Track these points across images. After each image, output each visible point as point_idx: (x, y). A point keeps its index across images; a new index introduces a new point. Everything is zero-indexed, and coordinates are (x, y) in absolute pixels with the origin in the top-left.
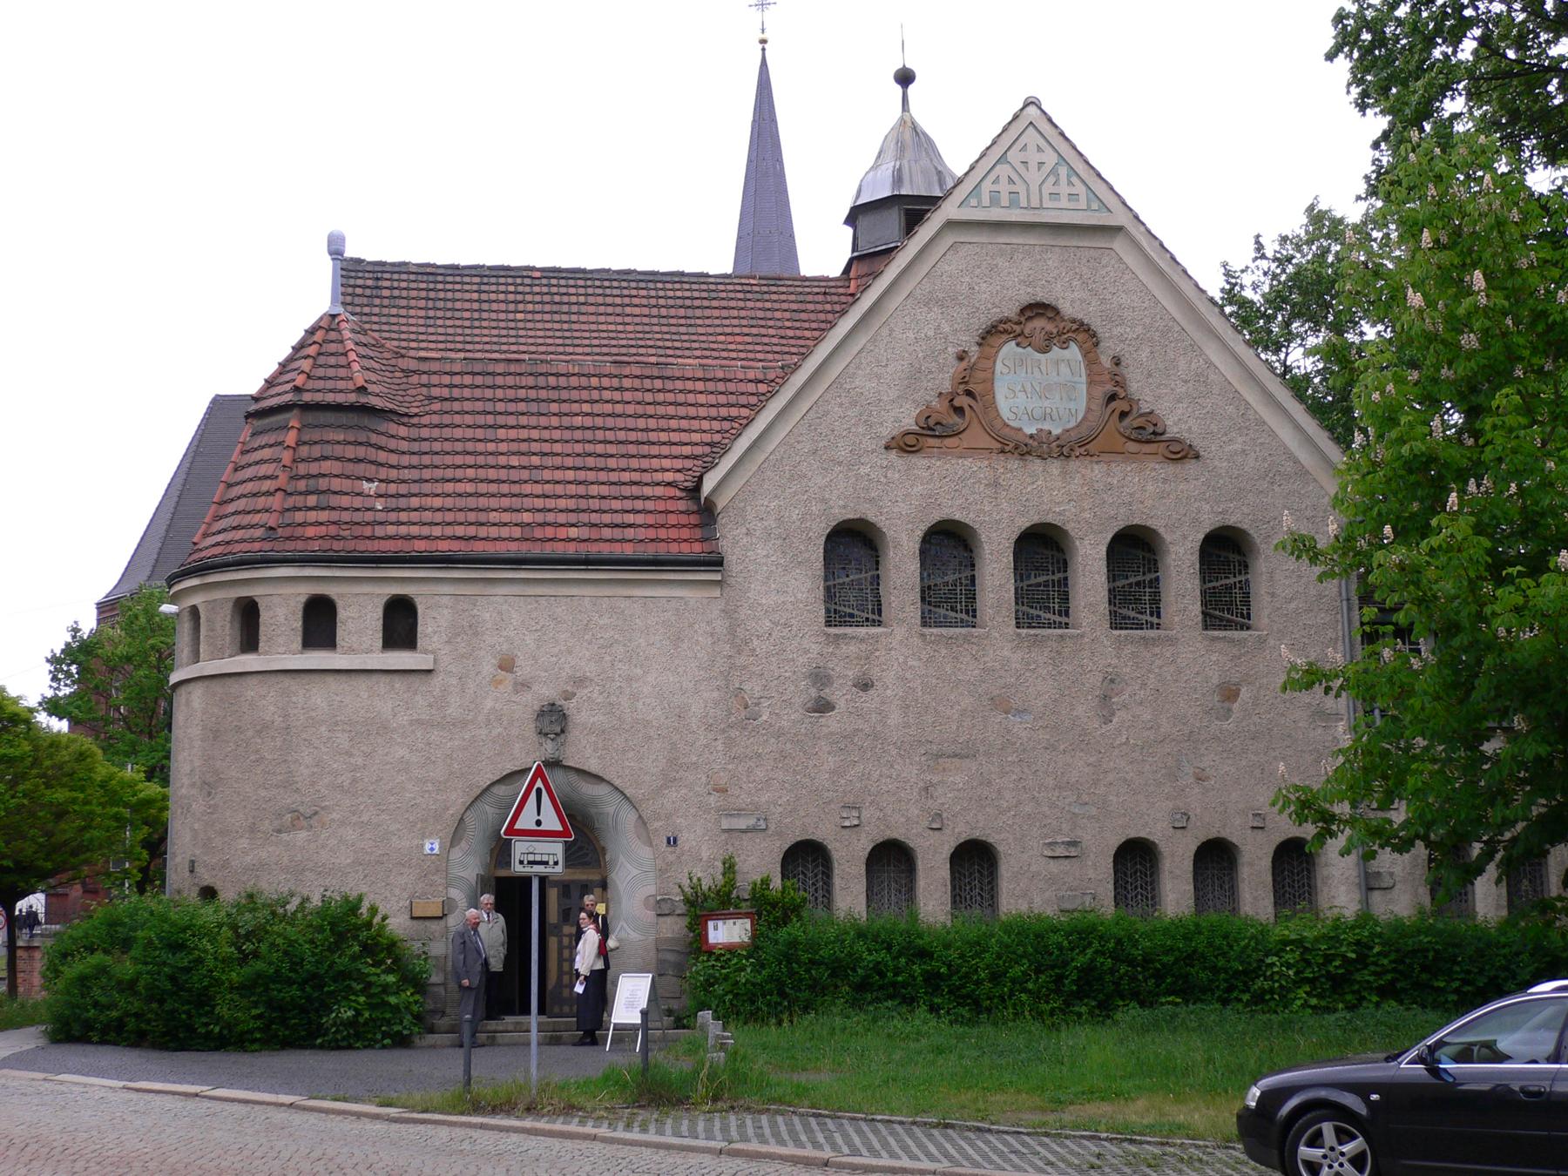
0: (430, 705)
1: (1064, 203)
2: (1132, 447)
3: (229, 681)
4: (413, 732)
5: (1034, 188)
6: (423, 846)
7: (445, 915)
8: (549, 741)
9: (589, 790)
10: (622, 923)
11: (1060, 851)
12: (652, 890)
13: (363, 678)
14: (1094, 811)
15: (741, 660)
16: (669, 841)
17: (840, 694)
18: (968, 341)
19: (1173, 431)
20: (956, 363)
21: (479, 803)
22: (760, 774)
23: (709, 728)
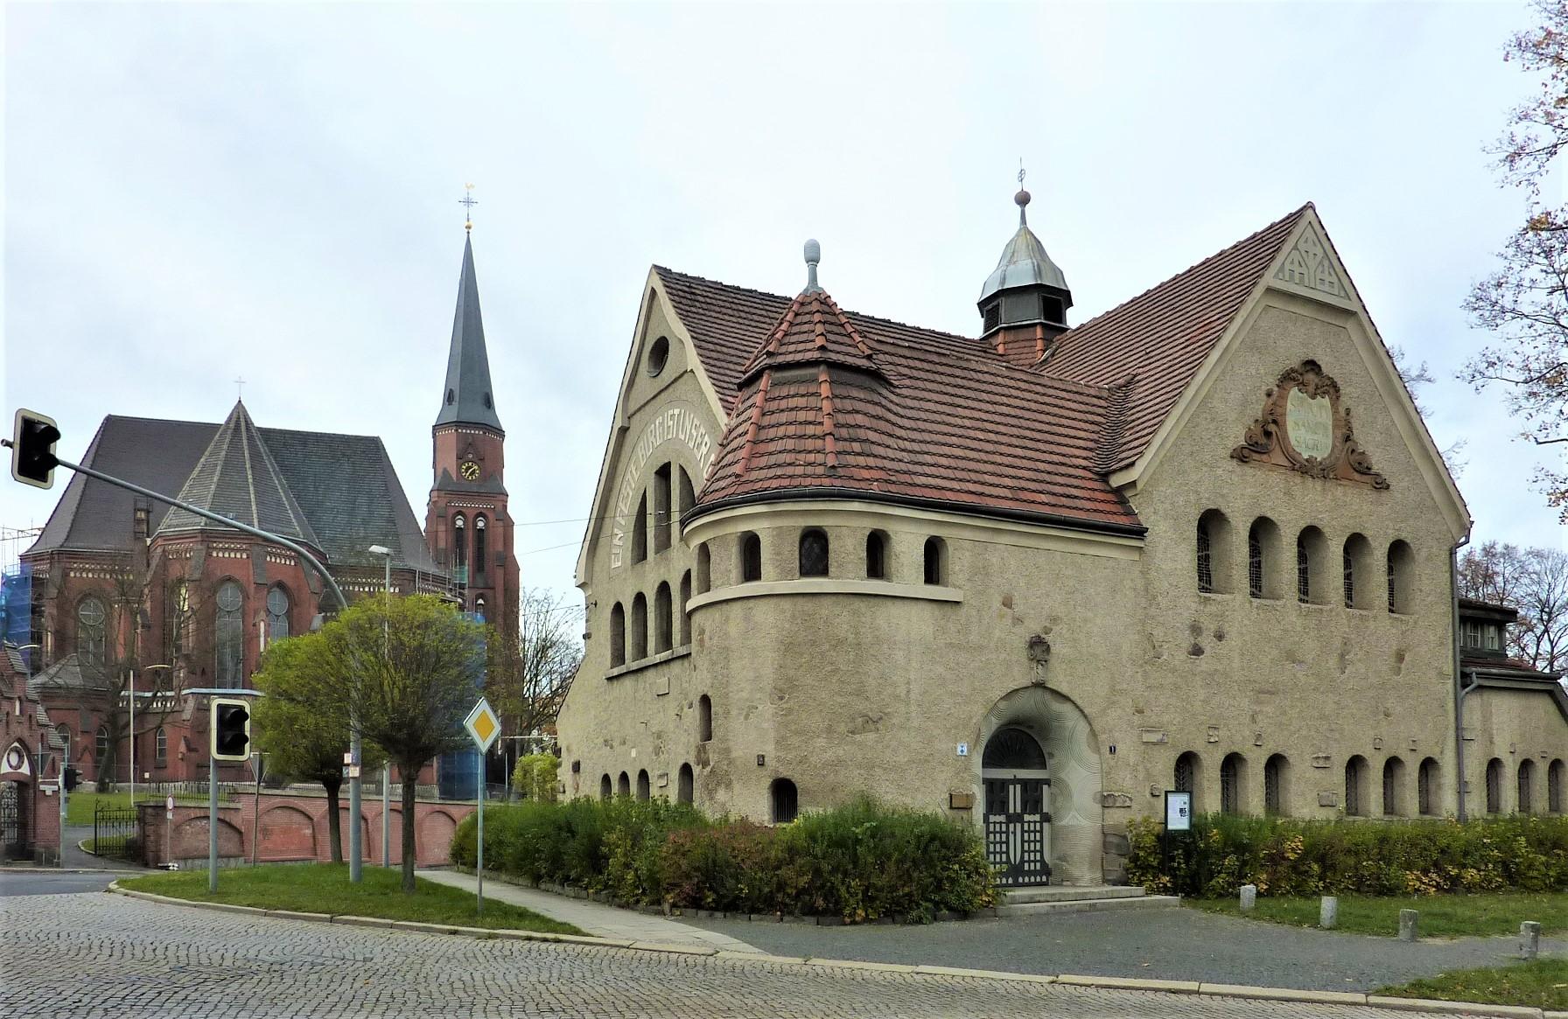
1: (1327, 288)
2: (1356, 476)
3: (725, 607)
5: (1312, 271)
9: (1058, 707)
11: (1321, 763)
13: (913, 603)
14: (1337, 736)
15: (1153, 611)
17: (1207, 642)
18: (1271, 382)
19: (1375, 468)
20: (1265, 398)
22: (1163, 700)
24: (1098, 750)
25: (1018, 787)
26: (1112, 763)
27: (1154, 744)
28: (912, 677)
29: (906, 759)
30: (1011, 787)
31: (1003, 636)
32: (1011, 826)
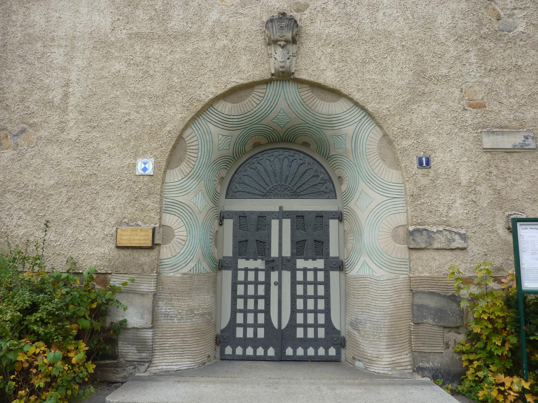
4: (132, 46)
6: (135, 165)
7: (154, 246)
8: (279, 50)
10: (364, 258)
12: (402, 219)
16: (420, 163)
21: (201, 121)
23: (459, 39)
24: (396, 164)
25: (287, 223)
26: (425, 181)
27: (509, 151)
28: (73, 77)
29: (52, 182)
30: (275, 223)
31: (224, 18)
32: (274, 275)
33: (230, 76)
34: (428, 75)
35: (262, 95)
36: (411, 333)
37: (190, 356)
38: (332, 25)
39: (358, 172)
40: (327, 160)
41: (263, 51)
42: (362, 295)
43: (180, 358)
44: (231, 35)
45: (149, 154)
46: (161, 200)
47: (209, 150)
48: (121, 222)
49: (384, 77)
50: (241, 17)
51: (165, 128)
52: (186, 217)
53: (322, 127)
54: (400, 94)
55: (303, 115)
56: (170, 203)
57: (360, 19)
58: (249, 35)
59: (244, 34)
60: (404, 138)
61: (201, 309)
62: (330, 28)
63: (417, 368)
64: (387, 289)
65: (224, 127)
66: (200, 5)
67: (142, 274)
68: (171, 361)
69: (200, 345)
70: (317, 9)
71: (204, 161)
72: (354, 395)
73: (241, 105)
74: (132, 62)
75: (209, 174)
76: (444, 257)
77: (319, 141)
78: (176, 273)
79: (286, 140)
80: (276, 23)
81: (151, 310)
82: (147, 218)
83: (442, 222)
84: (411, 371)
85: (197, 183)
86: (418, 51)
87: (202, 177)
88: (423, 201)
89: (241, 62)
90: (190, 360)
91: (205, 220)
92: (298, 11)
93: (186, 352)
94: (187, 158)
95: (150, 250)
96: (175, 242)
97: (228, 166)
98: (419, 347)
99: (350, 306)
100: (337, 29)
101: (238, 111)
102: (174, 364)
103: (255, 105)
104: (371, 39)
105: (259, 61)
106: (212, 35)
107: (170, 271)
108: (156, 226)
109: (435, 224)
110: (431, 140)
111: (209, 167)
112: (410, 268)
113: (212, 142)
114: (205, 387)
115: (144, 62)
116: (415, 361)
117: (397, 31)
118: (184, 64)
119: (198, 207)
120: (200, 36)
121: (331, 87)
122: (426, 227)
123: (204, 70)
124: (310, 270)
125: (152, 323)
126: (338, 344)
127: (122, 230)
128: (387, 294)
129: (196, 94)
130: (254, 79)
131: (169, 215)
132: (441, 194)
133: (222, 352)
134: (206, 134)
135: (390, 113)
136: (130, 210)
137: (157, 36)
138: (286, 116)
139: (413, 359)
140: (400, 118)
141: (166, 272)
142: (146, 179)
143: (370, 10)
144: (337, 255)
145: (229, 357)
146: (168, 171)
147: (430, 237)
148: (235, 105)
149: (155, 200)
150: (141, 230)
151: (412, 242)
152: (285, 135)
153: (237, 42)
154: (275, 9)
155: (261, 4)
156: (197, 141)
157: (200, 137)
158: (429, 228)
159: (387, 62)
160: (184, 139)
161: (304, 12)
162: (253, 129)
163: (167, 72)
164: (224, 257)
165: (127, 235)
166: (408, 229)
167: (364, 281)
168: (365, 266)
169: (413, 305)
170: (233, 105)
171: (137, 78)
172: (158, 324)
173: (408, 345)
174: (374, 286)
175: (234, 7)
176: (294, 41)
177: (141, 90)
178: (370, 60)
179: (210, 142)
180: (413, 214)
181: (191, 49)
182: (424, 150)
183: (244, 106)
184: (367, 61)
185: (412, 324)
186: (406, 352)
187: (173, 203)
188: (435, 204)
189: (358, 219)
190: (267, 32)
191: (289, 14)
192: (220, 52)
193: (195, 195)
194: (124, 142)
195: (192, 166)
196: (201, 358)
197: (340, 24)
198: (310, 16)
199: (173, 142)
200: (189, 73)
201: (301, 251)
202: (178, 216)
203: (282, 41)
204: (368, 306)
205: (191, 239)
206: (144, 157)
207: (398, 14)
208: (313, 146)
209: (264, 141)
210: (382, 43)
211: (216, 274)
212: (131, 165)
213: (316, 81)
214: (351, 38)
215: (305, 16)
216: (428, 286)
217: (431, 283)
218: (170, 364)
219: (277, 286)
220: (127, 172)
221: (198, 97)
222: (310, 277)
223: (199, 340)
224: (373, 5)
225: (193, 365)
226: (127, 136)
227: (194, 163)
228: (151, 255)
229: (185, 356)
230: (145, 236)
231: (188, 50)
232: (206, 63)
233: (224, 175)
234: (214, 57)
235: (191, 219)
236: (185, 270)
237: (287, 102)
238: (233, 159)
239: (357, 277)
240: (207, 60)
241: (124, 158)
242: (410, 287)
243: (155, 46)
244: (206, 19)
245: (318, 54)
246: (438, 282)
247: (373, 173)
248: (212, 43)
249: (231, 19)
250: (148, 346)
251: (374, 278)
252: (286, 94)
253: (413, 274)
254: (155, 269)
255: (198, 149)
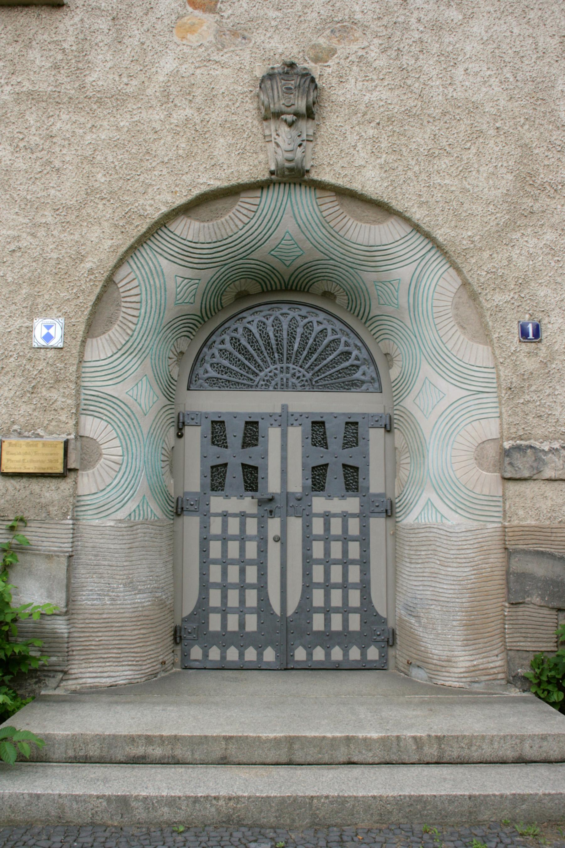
0: (56, 67)
4: (22, 115)
6: (30, 330)
8: (284, 129)
10: (429, 494)
16: (524, 333)
26: (530, 364)
33: (197, 174)
34: (539, 182)
35: (254, 208)
36: (504, 620)
37: (133, 661)
38: (376, 87)
39: (420, 347)
40: (365, 323)
41: (255, 130)
42: (424, 557)
43: (115, 664)
44: (199, 99)
45: (55, 310)
46: (78, 392)
47: (158, 304)
48: (8, 430)
49: (464, 182)
50: (216, 68)
51: (82, 265)
52: (121, 422)
53: (357, 266)
54: (492, 213)
55: (325, 245)
56: (92, 398)
57: (424, 78)
58: (230, 100)
59: (221, 97)
60: (497, 290)
61: (148, 582)
62: (373, 92)
63: (514, 677)
64: (465, 547)
65: (186, 264)
66: (143, 44)
67: (46, 521)
68: (100, 669)
69: (149, 643)
70: (350, 58)
71: (150, 324)
72: (411, 718)
73: (215, 225)
74: (21, 144)
75: (159, 346)
76: (560, 493)
77: (351, 291)
78: (104, 519)
79: (294, 288)
80: (279, 81)
81: (65, 582)
82: (54, 423)
83: (557, 435)
84: (503, 682)
85: (139, 362)
86: (522, 138)
87: (147, 351)
88: (527, 397)
89: (217, 149)
90: (134, 668)
91: (153, 428)
92: (316, 60)
93: (126, 655)
94: (120, 318)
95: (60, 480)
96: (103, 465)
97: (191, 333)
98: (517, 642)
99: (404, 576)
100: (385, 94)
101: (210, 236)
102: (106, 674)
103: (240, 225)
104: (444, 114)
105: (248, 148)
106: (165, 100)
107: (96, 516)
108: (69, 437)
109: (546, 438)
110: (542, 294)
111: (159, 333)
112: (504, 511)
113: (165, 291)
114: (163, 710)
115: (43, 144)
116: (511, 665)
117: (487, 102)
118: (116, 149)
119: (140, 405)
120: (144, 101)
121: (374, 197)
122: (532, 442)
123: (151, 161)
124: (335, 515)
125: (67, 606)
126: (383, 641)
127: (10, 444)
128: (465, 556)
129: (137, 205)
130: (240, 181)
131: (91, 418)
132: (558, 387)
133: (185, 655)
134: (155, 275)
135: (475, 246)
136: (24, 409)
137: (67, 99)
138: (296, 246)
139: (508, 662)
140: (491, 255)
141: (89, 517)
142: (51, 353)
143: (443, 63)
144: (381, 490)
145: (197, 664)
146: (89, 340)
147: (537, 459)
148: (206, 224)
149: (67, 392)
150: (44, 445)
151: (509, 468)
152: (293, 278)
153: (210, 112)
154: (277, 56)
155: (251, 45)
156: (139, 288)
157: (144, 281)
158: (537, 444)
159: (471, 156)
160: (116, 284)
161: (326, 62)
162: (237, 267)
163: (85, 163)
164: (185, 494)
165: (20, 454)
166: (502, 445)
167: (427, 534)
168: (430, 507)
169: (508, 573)
170: (202, 224)
171: (31, 172)
172: (76, 607)
173: (499, 640)
174: (445, 542)
175: (203, 49)
176: (310, 114)
177: (39, 196)
178: (441, 151)
179: (161, 289)
180: (511, 420)
181: (127, 124)
182: (530, 312)
183: (221, 226)
184: (437, 153)
185: (507, 604)
186: (496, 652)
187: (98, 396)
188: (548, 404)
189: (418, 427)
190: (262, 96)
191: (301, 65)
192: (178, 129)
193: (136, 383)
194: (10, 289)
195: (130, 332)
196: (150, 665)
197: (390, 87)
198: (337, 71)
199: (97, 290)
200: (124, 166)
201: (319, 483)
202: (106, 421)
203: (289, 114)
204: (435, 575)
205: (130, 460)
206: (46, 317)
207: (489, 72)
208: (341, 300)
209: (254, 288)
210: (461, 122)
211: (172, 522)
212: (23, 329)
213: (348, 187)
214: (410, 111)
215: (329, 70)
216: (534, 541)
217: (538, 537)
218: (99, 675)
219: (279, 544)
220: (16, 342)
221: (141, 211)
222: (336, 527)
223: (147, 635)
224: (447, 54)
225: (137, 676)
226: (16, 277)
227: (133, 327)
228: (62, 488)
229: (123, 661)
230: (51, 454)
231: (122, 124)
232: (154, 149)
233: (184, 348)
234: (169, 138)
235: (129, 425)
236: (122, 514)
237: (296, 220)
238: (200, 320)
239: (416, 526)
240: (156, 143)
241: (10, 317)
242: (505, 544)
243: (64, 117)
244: (154, 70)
245: (352, 138)
246: (549, 534)
247: (444, 349)
248: (165, 113)
249: (198, 71)
250: (61, 645)
251: (445, 529)
252: (295, 208)
253: (509, 521)
254: (70, 513)
255: (140, 302)
